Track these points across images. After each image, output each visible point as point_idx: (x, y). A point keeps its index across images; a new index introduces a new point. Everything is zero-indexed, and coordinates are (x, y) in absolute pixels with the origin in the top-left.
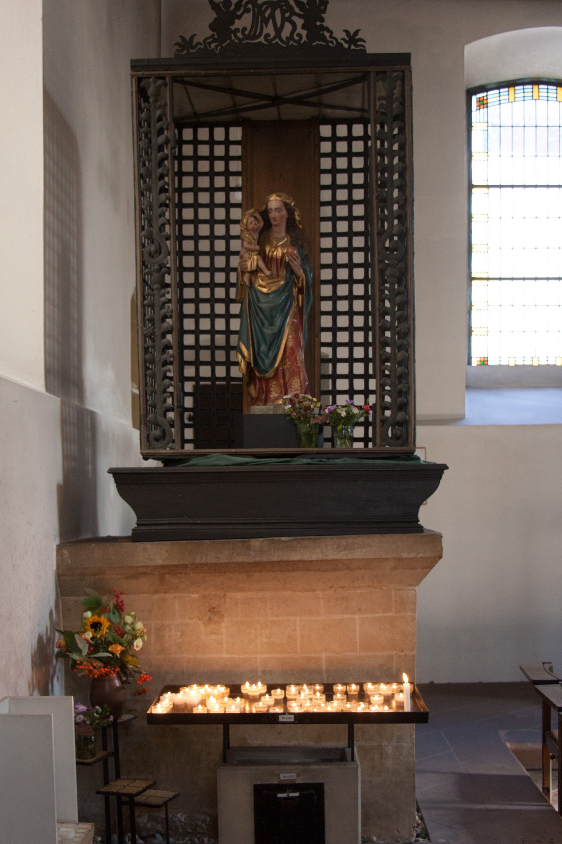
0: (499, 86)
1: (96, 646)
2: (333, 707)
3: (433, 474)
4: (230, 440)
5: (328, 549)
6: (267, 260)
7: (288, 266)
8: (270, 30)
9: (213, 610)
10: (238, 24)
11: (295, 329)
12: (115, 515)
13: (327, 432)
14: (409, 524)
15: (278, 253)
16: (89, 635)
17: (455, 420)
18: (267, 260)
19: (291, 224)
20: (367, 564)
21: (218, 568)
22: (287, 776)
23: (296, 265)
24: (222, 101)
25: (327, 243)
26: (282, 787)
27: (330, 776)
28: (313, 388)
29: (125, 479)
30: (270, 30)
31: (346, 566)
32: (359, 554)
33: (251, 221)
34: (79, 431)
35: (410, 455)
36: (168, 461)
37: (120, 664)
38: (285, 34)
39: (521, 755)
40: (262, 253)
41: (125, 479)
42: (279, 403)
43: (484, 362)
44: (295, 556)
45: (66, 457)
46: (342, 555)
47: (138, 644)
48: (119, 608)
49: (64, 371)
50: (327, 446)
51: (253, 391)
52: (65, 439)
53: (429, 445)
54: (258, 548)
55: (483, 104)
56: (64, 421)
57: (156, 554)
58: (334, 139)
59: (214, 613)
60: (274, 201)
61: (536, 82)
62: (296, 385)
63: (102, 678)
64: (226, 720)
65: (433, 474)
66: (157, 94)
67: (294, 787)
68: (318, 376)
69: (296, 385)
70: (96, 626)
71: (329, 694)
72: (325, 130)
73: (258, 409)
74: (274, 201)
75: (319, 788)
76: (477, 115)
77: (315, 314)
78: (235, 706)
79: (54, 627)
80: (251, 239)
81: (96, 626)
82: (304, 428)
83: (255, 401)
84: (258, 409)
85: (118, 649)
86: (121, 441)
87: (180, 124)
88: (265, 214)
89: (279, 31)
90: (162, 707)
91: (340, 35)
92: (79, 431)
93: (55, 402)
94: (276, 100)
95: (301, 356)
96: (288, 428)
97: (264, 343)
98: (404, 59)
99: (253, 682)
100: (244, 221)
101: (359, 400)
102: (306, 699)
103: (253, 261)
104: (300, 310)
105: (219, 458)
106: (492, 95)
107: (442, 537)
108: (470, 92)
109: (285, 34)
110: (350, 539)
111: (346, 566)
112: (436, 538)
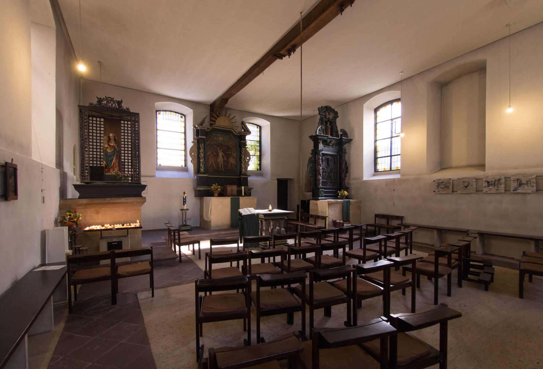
0: (163, 111)
1: (70, 219)
2: (124, 227)
3: (144, 187)
4: (101, 179)
5: (123, 200)
6: (110, 146)
7: (114, 147)
8: (110, 104)
9: (97, 212)
10: (103, 102)
11: (116, 159)
12: (72, 193)
13: (123, 178)
14: (140, 195)
15: (112, 145)
16: (69, 217)
17: (155, 176)
18: (110, 146)
19: (115, 140)
20: (131, 203)
21: (98, 204)
22: (114, 240)
23: (116, 147)
24: (100, 114)
25: (122, 134)
26: (113, 242)
27: (123, 240)
28: (120, 170)
29: (76, 187)
30: (110, 104)
31: (127, 203)
32: (130, 201)
33: (106, 138)
34: (64, 177)
35: (140, 183)
36: (86, 183)
37: (76, 223)
38: (114, 105)
39: (165, 239)
40: (108, 144)
41: (76, 187)
42: (113, 173)
43: (160, 165)
44: (116, 201)
45: (61, 182)
46: (126, 201)
47: (80, 218)
48: (75, 212)
49: (60, 164)
50: (123, 181)
51: (106, 170)
52: (61, 178)
53: (143, 181)
54: (108, 200)
55: (159, 113)
56: (61, 175)
57: (85, 201)
58: (124, 124)
59: (98, 212)
60: (111, 135)
61: (171, 111)
62: (116, 169)
63: (72, 225)
64: (101, 230)
65: (144, 187)
66: (84, 113)
67: (116, 242)
68: (121, 166)
69: (116, 169)
70: (70, 215)
71: (123, 225)
72: (122, 122)
73: (107, 174)
74: (111, 135)
75: (121, 242)
76: (158, 116)
77: (120, 156)
78: (103, 228)
79: (58, 216)
80: (106, 142)
81: (70, 215)
82: (118, 178)
83: (106, 172)
84: (107, 174)
85: (76, 220)
86: (74, 178)
87: (89, 116)
88: (109, 137)
89: (112, 105)
90: (87, 229)
91: (125, 108)
92: (64, 177)
93: (58, 171)
94: (111, 116)
95: (117, 164)
96: (114, 178)
97: (109, 161)
98: (138, 114)
99: (107, 224)
100: (104, 139)
101: (130, 173)
102: (118, 226)
103: (106, 146)
104: (117, 156)
105: (99, 183)
106: (162, 112)
107: (15, 169)
108: (157, 111)
109: (114, 105)
110: (126, 198)
111: (127, 203)
112: (145, 198)
